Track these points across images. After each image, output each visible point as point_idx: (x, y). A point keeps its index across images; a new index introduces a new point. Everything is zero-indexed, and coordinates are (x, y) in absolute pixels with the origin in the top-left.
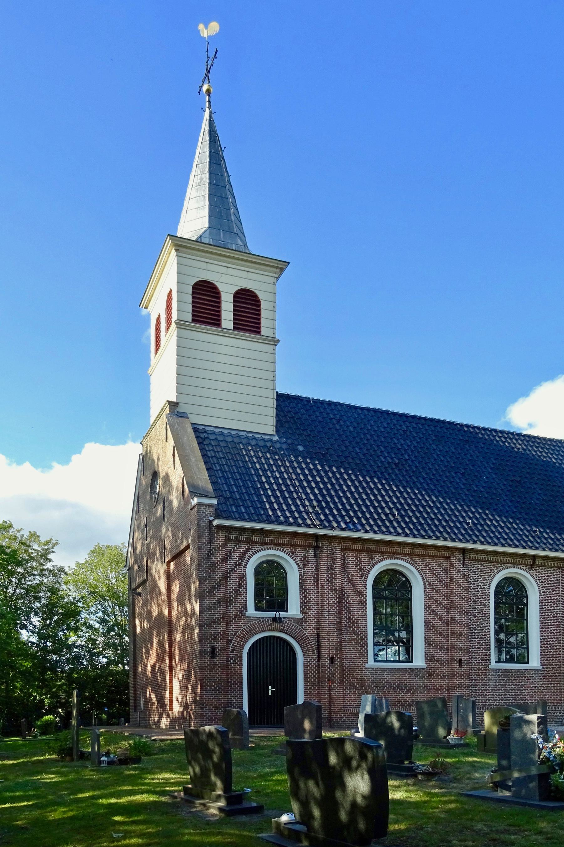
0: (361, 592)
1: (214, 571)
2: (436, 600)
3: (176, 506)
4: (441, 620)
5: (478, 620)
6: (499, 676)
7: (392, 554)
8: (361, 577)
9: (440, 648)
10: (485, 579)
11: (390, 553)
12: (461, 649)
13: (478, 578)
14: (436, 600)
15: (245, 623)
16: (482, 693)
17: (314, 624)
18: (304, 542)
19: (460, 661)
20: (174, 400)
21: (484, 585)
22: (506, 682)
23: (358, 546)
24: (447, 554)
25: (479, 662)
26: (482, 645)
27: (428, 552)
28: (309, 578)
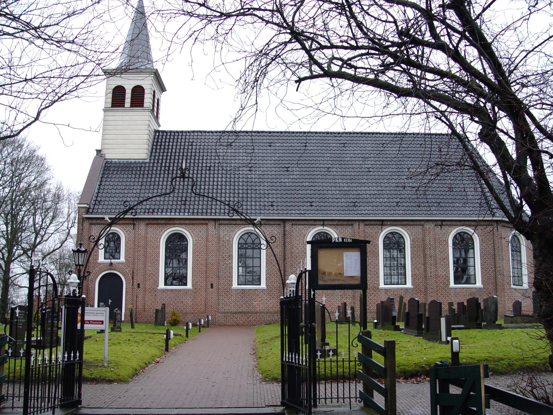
0: (157, 247)
1: (83, 240)
2: (200, 249)
3: (533, 176)
4: (202, 260)
5: (225, 259)
6: (238, 293)
7: (174, 224)
8: (157, 239)
9: (201, 277)
10: (230, 235)
11: (174, 224)
12: (212, 278)
13: (226, 235)
14: (200, 249)
15: (97, 266)
16: (227, 304)
17: (131, 266)
18: (127, 222)
19: (212, 285)
20: (100, 149)
21: (230, 239)
22: (243, 297)
23: (155, 222)
24: (206, 222)
25: (225, 285)
26: (227, 275)
27: (415, 223)
28: (130, 241)
